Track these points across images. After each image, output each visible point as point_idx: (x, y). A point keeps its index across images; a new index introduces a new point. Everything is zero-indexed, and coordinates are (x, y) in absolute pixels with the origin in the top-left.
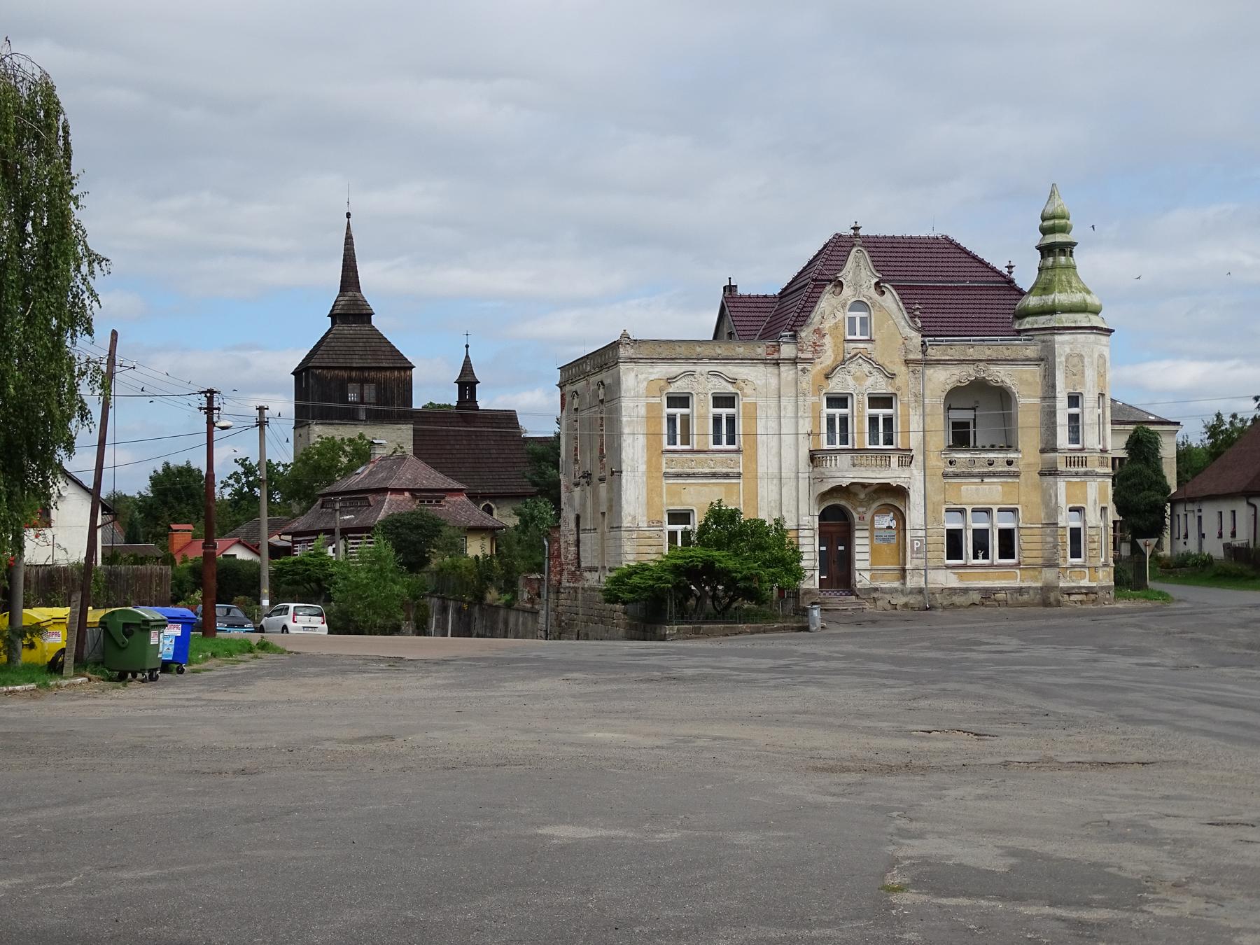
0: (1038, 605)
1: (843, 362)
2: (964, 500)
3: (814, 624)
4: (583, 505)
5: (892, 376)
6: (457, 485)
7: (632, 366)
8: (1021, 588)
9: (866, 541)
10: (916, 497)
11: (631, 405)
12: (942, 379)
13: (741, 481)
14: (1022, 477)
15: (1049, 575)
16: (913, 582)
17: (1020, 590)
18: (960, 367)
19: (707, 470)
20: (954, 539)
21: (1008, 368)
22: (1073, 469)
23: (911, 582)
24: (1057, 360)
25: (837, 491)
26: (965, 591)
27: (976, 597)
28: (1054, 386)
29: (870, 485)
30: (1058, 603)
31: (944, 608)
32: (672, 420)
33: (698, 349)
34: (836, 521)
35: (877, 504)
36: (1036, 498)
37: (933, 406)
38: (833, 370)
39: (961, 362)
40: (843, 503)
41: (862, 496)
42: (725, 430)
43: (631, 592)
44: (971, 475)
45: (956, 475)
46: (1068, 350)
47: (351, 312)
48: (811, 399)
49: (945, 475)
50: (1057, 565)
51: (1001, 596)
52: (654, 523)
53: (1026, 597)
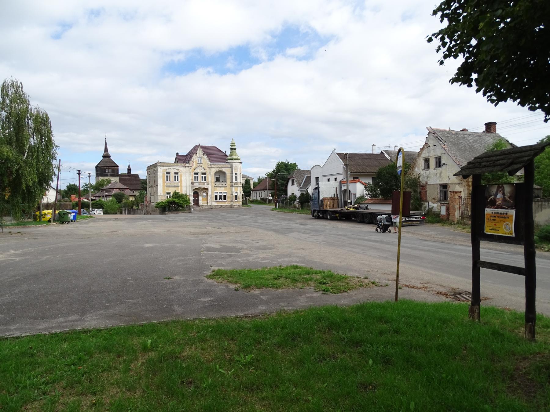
10: (210, 190)
12: (214, 170)
15: (232, 203)
16: (209, 204)
20: (216, 197)
32: (167, 176)
34: (196, 194)
42: (177, 178)
47: (106, 156)
52: (164, 194)
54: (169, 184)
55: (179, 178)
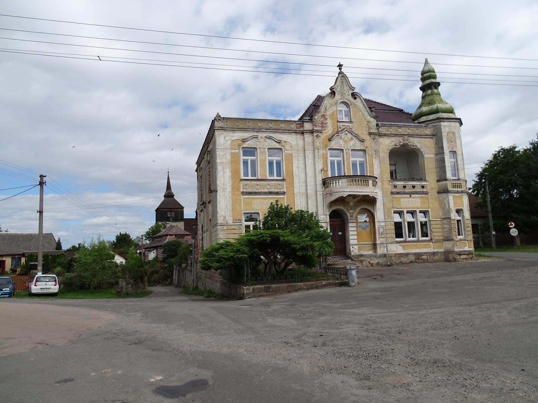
0: (443, 261)
1: (338, 132)
2: (402, 206)
3: (353, 281)
5: (362, 141)
6: (188, 233)
7: (222, 132)
8: (434, 253)
9: (355, 229)
10: (379, 205)
11: (222, 153)
12: (387, 144)
13: (285, 196)
14: (429, 194)
15: (448, 245)
16: (381, 251)
17: (434, 254)
18: (395, 138)
19: (266, 190)
20: (398, 226)
21: (418, 139)
23: (381, 251)
24: (443, 134)
25: (341, 200)
26: (407, 255)
27: (412, 258)
28: (442, 148)
29: (359, 196)
30: (455, 260)
31: (397, 264)
32: (245, 163)
33: (259, 124)
34: (338, 218)
35: (358, 209)
36: (437, 205)
37: (383, 157)
38: (333, 136)
39: (396, 135)
40: (341, 208)
41: (352, 204)
43: (218, 261)
44: (405, 193)
45: (398, 193)
46: (447, 129)
47: (169, 195)
48: (322, 152)
49: (392, 193)
50: (453, 240)
51: (424, 257)
52: (237, 221)
53: (437, 257)
55: (284, 168)
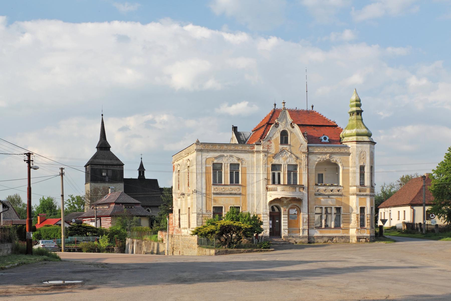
2: (322, 204)
4: (181, 205)
5: (297, 158)
6: (139, 202)
22: (362, 193)
25: (276, 200)
26: (322, 237)
27: (326, 239)
35: (290, 206)
42: (235, 178)
47: (103, 146)
54: (220, 189)
